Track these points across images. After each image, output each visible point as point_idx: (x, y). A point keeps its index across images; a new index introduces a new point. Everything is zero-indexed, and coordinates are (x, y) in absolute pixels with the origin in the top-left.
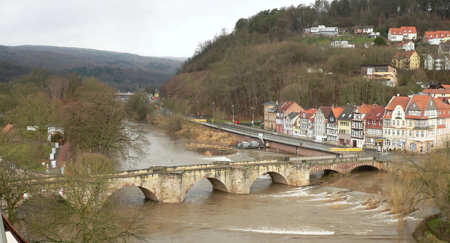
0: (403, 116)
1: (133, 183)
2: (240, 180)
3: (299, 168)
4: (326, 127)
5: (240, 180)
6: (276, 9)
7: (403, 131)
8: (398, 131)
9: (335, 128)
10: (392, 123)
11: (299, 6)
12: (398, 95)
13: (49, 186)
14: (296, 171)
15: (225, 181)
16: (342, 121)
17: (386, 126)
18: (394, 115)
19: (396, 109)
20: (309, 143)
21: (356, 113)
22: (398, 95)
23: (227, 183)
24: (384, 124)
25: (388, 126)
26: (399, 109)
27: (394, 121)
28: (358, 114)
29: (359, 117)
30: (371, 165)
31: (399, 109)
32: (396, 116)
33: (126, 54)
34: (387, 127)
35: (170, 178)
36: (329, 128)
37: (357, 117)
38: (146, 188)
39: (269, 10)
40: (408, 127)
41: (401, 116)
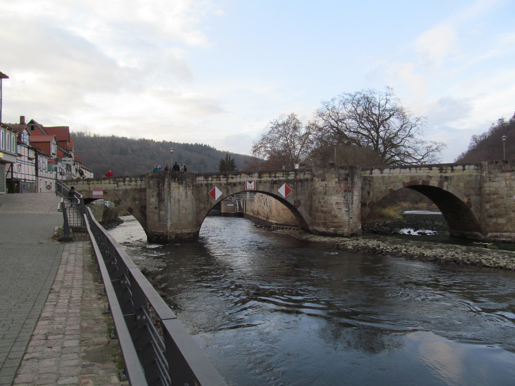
1: (425, 178)
13: (260, 177)
35: (503, 171)
38: (451, 190)
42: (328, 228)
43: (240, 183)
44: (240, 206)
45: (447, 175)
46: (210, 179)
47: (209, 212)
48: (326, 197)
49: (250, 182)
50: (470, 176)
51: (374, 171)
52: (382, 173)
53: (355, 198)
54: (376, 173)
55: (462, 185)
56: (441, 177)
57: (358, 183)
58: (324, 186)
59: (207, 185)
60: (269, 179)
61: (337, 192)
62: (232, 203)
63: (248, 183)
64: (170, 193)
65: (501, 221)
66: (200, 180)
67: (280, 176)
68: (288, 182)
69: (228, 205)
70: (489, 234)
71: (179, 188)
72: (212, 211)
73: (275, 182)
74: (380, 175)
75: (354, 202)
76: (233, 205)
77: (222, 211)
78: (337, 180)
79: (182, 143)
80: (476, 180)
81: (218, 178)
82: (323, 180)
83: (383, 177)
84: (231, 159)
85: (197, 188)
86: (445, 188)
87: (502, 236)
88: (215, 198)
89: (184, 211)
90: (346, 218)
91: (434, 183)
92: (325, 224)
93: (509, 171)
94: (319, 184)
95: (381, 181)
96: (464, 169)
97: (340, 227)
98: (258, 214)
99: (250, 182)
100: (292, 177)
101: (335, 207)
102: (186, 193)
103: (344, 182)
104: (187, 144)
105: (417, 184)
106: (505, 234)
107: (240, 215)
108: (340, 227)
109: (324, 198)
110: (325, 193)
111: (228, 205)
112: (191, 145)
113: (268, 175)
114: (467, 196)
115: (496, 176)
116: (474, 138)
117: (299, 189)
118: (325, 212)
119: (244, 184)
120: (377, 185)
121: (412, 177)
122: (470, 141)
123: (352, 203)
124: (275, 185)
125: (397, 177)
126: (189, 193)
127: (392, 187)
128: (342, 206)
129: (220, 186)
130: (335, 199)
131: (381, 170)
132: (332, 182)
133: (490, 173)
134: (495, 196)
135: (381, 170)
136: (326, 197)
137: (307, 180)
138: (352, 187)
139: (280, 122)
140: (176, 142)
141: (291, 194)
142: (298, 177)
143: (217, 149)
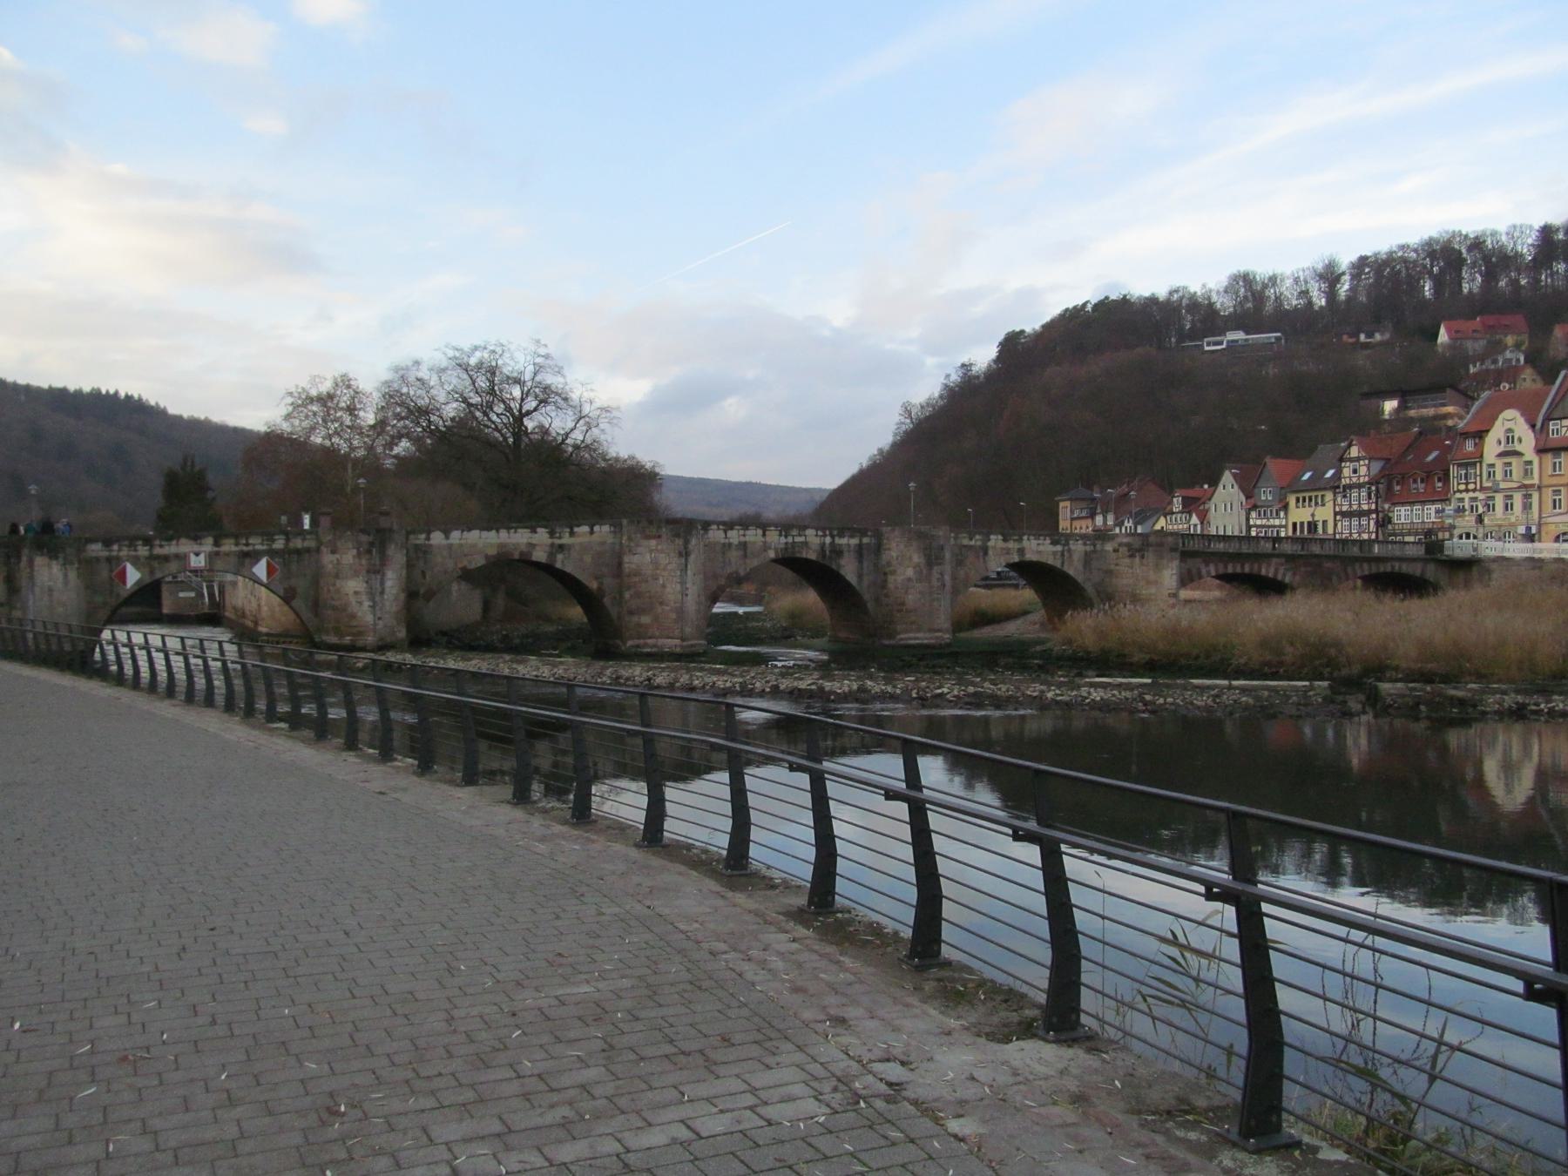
0: (1527, 442)
1: (523, 548)
2: (910, 572)
3: (1139, 550)
4: (1248, 520)
5: (910, 572)
7: (1528, 496)
8: (1511, 497)
9: (1277, 522)
11: (1171, 293)
13: (216, 544)
14: (1127, 561)
15: (860, 576)
16: (1301, 495)
18: (1492, 447)
23: (866, 580)
24: (1454, 483)
26: (1510, 421)
27: (1492, 465)
28: (1358, 459)
29: (1363, 470)
30: (1418, 573)
31: (1510, 421)
32: (1502, 448)
33: (749, 484)
34: (1467, 491)
35: (648, 537)
36: (1259, 522)
37: (1355, 471)
38: (568, 569)
39: (1085, 305)
40: (1546, 481)
41: (1518, 447)
42: (341, 635)
43: (177, 556)
44: (211, 595)
46: (115, 547)
47: (114, 611)
48: (338, 583)
49: (197, 554)
50: (603, 543)
51: (433, 535)
52: (447, 538)
53: (389, 584)
54: (437, 538)
55: (588, 559)
56: (552, 545)
57: (397, 557)
59: (109, 560)
60: (234, 548)
61: (356, 574)
62: (192, 589)
63: (193, 557)
64: (31, 577)
65: (645, 619)
66: (96, 549)
67: (257, 543)
68: (272, 553)
69: (182, 595)
70: (630, 643)
71: (49, 566)
72: (124, 610)
73: (246, 555)
74: (445, 542)
75: (387, 590)
76: (193, 594)
77: (165, 611)
79: (45, 386)
81: (132, 546)
82: (333, 552)
83: (450, 546)
84: (197, 468)
85: (88, 566)
86: (558, 565)
87: (646, 645)
88: (124, 582)
89: (61, 609)
90: (369, 618)
91: (540, 556)
92: (338, 632)
94: (328, 559)
95: (445, 553)
96: (592, 532)
97: (360, 633)
98: (244, 615)
99: (197, 554)
100: (279, 544)
101: (353, 599)
102: (66, 576)
104: (64, 391)
106: (650, 641)
107: (213, 618)
108: (360, 633)
111: (182, 595)
112: (79, 393)
113: (232, 541)
114: (596, 578)
116: (908, 412)
117: (294, 567)
119: (182, 558)
120: (439, 559)
121: (501, 546)
122: (897, 418)
123: (382, 593)
124: (247, 561)
125: (474, 546)
126: (72, 575)
127: (465, 563)
128: (364, 597)
129: (136, 562)
130: (353, 586)
131: (447, 534)
132: (348, 557)
133: (630, 539)
134: (636, 579)
135: (447, 534)
136: (338, 583)
137: (308, 550)
138: (383, 564)
139: (314, 393)
140: (22, 381)
141: (277, 575)
142: (291, 545)
143: (172, 411)
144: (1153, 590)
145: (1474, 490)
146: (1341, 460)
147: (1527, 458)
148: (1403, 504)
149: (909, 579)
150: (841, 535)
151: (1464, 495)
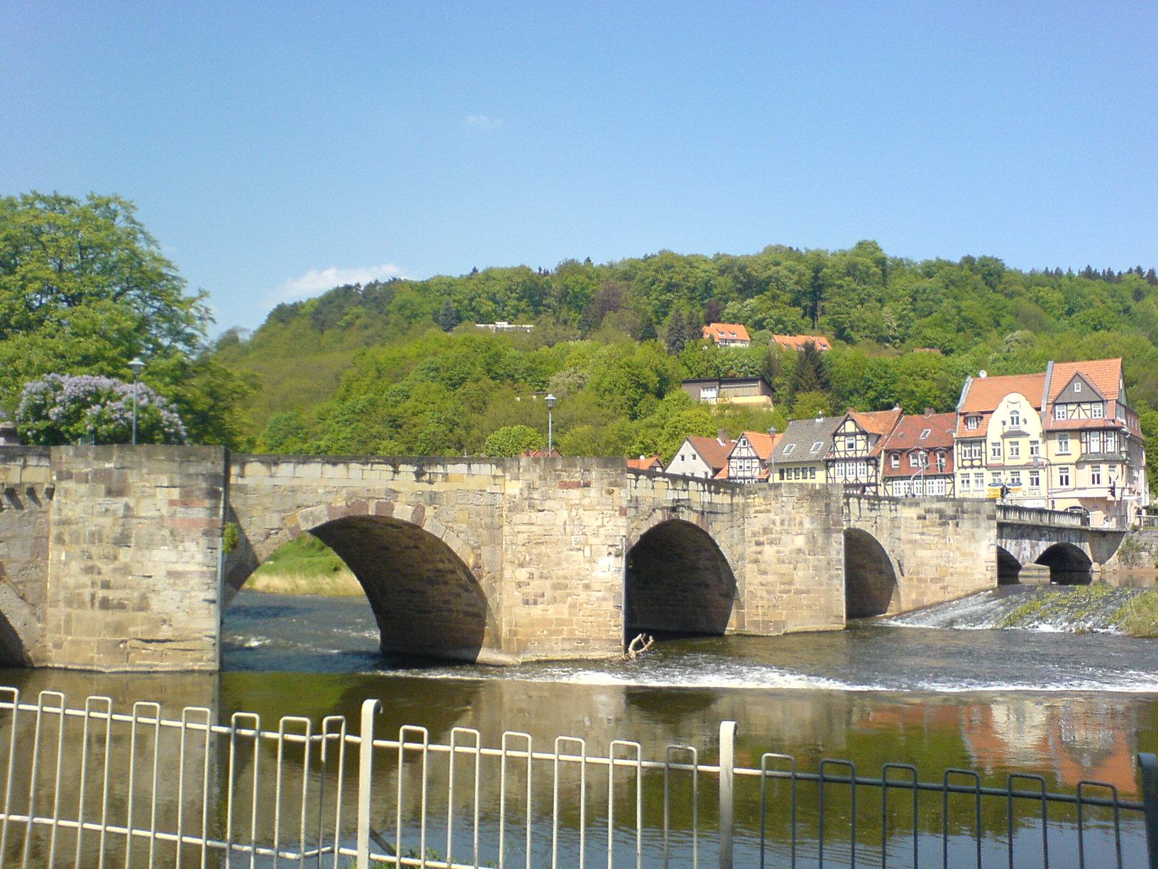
0: (1034, 427)
2: (800, 541)
5: (800, 541)
6: (377, 281)
10: (990, 453)
12: (983, 374)
17: (967, 463)
18: (994, 428)
19: (1002, 406)
20: (216, 790)
21: (846, 435)
22: (983, 374)
25: (976, 463)
28: (855, 434)
32: (1006, 429)
34: (972, 467)
39: (358, 285)
40: (1054, 460)
41: (1023, 428)
45: (434, 488)
48: (125, 555)
58: (121, 512)
74: (270, 482)
78: (175, 494)
80: (243, 465)
93: (578, 485)
103: (207, 503)
105: (363, 513)
109: (115, 558)
110: (122, 541)
115: (546, 498)
118: (121, 606)
144: (969, 563)
145: (981, 466)
146: (835, 435)
147: (1033, 438)
148: (902, 478)
149: (799, 551)
150: (717, 492)
151: (968, 471)
